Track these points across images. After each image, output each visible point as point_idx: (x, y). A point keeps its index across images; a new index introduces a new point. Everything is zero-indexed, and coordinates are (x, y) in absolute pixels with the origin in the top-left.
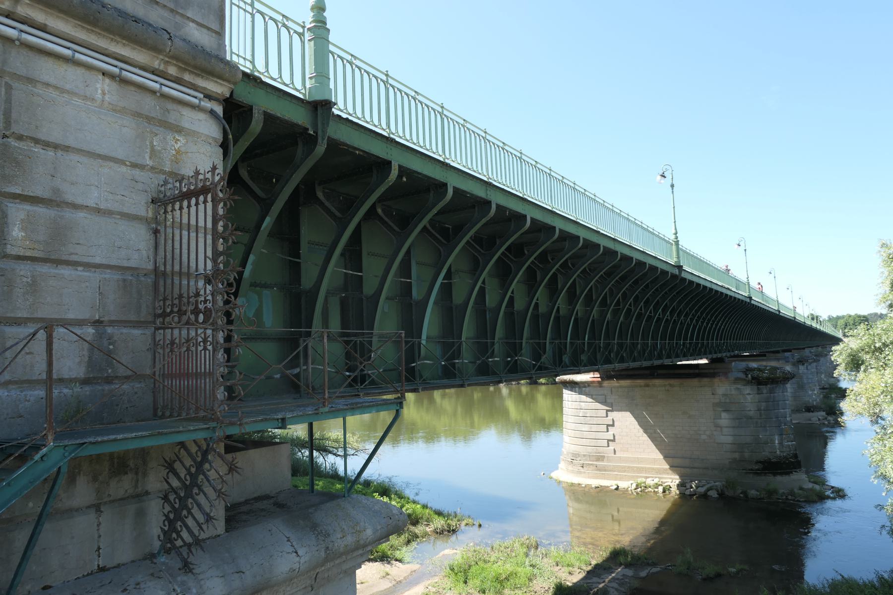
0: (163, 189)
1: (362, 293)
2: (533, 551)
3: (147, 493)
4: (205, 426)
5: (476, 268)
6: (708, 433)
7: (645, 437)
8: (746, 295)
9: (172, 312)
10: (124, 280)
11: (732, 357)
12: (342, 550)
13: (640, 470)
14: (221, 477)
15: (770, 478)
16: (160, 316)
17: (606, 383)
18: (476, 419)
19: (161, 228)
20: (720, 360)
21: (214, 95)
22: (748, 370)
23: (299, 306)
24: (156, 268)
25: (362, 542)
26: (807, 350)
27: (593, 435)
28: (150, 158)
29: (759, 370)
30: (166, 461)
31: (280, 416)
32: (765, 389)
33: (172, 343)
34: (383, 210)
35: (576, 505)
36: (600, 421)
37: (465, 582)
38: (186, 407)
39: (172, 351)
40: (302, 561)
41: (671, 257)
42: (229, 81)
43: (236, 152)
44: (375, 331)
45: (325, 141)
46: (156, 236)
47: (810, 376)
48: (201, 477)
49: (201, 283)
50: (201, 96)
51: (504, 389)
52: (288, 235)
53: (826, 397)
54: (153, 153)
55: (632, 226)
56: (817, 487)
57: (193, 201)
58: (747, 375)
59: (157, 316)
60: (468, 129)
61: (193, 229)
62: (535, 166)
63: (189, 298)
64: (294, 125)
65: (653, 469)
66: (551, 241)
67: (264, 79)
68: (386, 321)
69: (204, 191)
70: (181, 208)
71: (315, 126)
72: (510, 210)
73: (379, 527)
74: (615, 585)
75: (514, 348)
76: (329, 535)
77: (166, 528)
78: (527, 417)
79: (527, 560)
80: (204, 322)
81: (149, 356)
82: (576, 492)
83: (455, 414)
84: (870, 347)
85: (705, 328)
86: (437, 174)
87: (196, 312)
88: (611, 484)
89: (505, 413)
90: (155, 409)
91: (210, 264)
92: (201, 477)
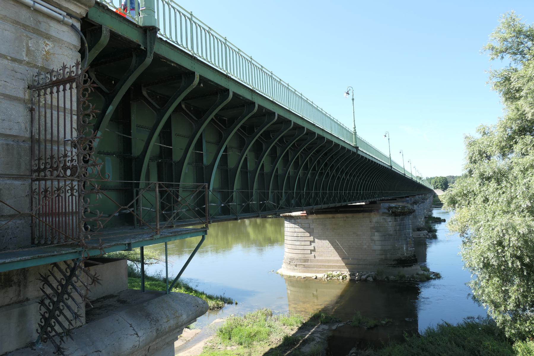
0: (37, 79)
1: (172, 159)
2: (269, 317)
3: (27, 300)
4: (74, 251)
5: (242, 146)
6: (367, 244)
7: (332, 248)
8: (389, 165)
9: (45, 168)
10: (7, 145)
11: (381, 200)
12: (167, 330)
13: (329, 267)
14: (86, 287)
15: (401, 269)
16: (35, 171)
17: (310, 217)
18: (230, 238)
19: (36, 107)
20: (374, 203)
21: (74, 14)
22: (390, 208)
23: (130, 166)
24: (32, 137)
25: (180, 324)
26: (417, 196)
27: (302, 247)
28: (27, 55)
29: (396, 208)
30: (42, 276)
31: (127, 242)
32: (399, 219)
33: (46, 191)
34: (185, 106)
35: (292, 289)
36: (306, 239)
37: (230, 339)
38: (57, 237)
39: (45, 196)
40: (141, 340)
41: (352, 142)
42: (85, 5)
43: (91, 56)
44: (181, 183)
45: (152, 55)
46: (32, 113)
47: (420, 211)
48: (70, 287)
49: (69, 148)
50: (65, 14)
51: (247, 221)
52: (122, 120)
53: (427, 222)
54: (29, 52)
55: (333, 123)
56: (426, 273)
57: (61, 87)
58: (389, 211)
59: (33, 171)
60: (241, 55)
61: (61, 109)
62: (280, 82)
63: (59, 158)
64: (130, 42)
65: (337, 266)
66: (289, 129)
67: (109, 7)
68: (187, 178)
69: (70, 80)
70: (51, 93)
71: (145, 44)
72: (266, 109)
73: (190, 313)
74: (318, 335)
75: (264, 196)
76: (158, 321)
77: (43, 324)
78: (261, 238)
79: (266, 323)
80: (71, 175)
81: (28, 200)
82: (292, 281)
83: (217, 236)
84: (461, 193)
85: (362, 183)
86: (223, 83)
87: (65, 168)
88: (312, 275)
89: (248, 235)
90: (33, 239)
91: (75, 134)
92: (70, 287)
